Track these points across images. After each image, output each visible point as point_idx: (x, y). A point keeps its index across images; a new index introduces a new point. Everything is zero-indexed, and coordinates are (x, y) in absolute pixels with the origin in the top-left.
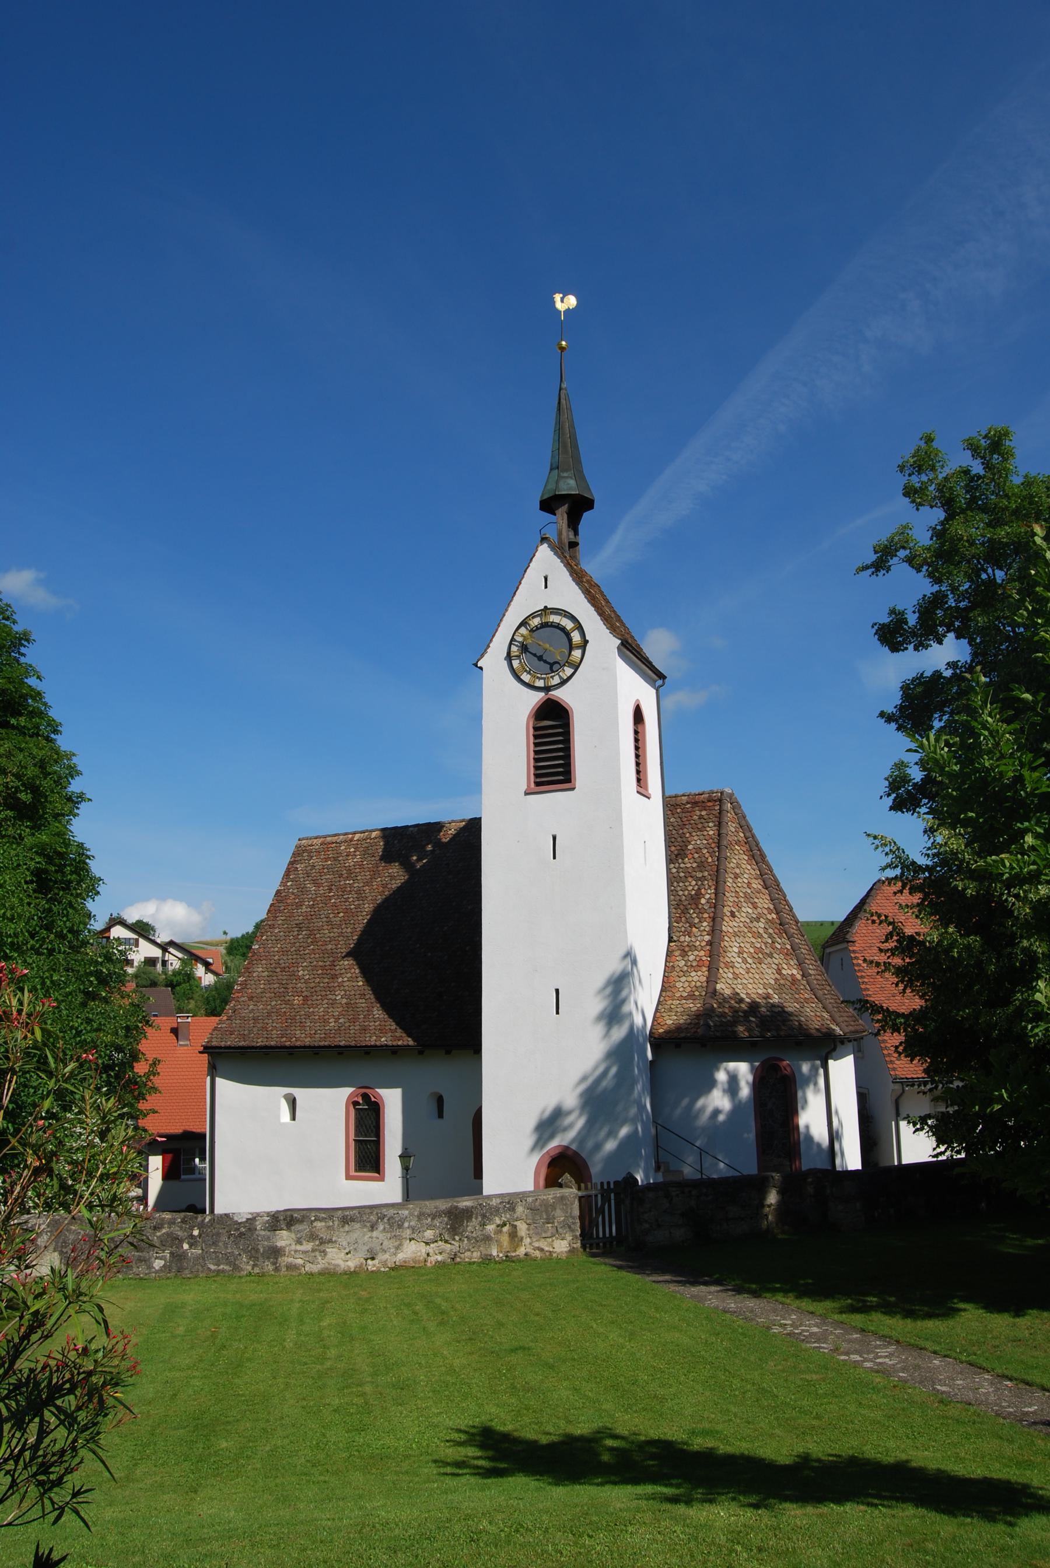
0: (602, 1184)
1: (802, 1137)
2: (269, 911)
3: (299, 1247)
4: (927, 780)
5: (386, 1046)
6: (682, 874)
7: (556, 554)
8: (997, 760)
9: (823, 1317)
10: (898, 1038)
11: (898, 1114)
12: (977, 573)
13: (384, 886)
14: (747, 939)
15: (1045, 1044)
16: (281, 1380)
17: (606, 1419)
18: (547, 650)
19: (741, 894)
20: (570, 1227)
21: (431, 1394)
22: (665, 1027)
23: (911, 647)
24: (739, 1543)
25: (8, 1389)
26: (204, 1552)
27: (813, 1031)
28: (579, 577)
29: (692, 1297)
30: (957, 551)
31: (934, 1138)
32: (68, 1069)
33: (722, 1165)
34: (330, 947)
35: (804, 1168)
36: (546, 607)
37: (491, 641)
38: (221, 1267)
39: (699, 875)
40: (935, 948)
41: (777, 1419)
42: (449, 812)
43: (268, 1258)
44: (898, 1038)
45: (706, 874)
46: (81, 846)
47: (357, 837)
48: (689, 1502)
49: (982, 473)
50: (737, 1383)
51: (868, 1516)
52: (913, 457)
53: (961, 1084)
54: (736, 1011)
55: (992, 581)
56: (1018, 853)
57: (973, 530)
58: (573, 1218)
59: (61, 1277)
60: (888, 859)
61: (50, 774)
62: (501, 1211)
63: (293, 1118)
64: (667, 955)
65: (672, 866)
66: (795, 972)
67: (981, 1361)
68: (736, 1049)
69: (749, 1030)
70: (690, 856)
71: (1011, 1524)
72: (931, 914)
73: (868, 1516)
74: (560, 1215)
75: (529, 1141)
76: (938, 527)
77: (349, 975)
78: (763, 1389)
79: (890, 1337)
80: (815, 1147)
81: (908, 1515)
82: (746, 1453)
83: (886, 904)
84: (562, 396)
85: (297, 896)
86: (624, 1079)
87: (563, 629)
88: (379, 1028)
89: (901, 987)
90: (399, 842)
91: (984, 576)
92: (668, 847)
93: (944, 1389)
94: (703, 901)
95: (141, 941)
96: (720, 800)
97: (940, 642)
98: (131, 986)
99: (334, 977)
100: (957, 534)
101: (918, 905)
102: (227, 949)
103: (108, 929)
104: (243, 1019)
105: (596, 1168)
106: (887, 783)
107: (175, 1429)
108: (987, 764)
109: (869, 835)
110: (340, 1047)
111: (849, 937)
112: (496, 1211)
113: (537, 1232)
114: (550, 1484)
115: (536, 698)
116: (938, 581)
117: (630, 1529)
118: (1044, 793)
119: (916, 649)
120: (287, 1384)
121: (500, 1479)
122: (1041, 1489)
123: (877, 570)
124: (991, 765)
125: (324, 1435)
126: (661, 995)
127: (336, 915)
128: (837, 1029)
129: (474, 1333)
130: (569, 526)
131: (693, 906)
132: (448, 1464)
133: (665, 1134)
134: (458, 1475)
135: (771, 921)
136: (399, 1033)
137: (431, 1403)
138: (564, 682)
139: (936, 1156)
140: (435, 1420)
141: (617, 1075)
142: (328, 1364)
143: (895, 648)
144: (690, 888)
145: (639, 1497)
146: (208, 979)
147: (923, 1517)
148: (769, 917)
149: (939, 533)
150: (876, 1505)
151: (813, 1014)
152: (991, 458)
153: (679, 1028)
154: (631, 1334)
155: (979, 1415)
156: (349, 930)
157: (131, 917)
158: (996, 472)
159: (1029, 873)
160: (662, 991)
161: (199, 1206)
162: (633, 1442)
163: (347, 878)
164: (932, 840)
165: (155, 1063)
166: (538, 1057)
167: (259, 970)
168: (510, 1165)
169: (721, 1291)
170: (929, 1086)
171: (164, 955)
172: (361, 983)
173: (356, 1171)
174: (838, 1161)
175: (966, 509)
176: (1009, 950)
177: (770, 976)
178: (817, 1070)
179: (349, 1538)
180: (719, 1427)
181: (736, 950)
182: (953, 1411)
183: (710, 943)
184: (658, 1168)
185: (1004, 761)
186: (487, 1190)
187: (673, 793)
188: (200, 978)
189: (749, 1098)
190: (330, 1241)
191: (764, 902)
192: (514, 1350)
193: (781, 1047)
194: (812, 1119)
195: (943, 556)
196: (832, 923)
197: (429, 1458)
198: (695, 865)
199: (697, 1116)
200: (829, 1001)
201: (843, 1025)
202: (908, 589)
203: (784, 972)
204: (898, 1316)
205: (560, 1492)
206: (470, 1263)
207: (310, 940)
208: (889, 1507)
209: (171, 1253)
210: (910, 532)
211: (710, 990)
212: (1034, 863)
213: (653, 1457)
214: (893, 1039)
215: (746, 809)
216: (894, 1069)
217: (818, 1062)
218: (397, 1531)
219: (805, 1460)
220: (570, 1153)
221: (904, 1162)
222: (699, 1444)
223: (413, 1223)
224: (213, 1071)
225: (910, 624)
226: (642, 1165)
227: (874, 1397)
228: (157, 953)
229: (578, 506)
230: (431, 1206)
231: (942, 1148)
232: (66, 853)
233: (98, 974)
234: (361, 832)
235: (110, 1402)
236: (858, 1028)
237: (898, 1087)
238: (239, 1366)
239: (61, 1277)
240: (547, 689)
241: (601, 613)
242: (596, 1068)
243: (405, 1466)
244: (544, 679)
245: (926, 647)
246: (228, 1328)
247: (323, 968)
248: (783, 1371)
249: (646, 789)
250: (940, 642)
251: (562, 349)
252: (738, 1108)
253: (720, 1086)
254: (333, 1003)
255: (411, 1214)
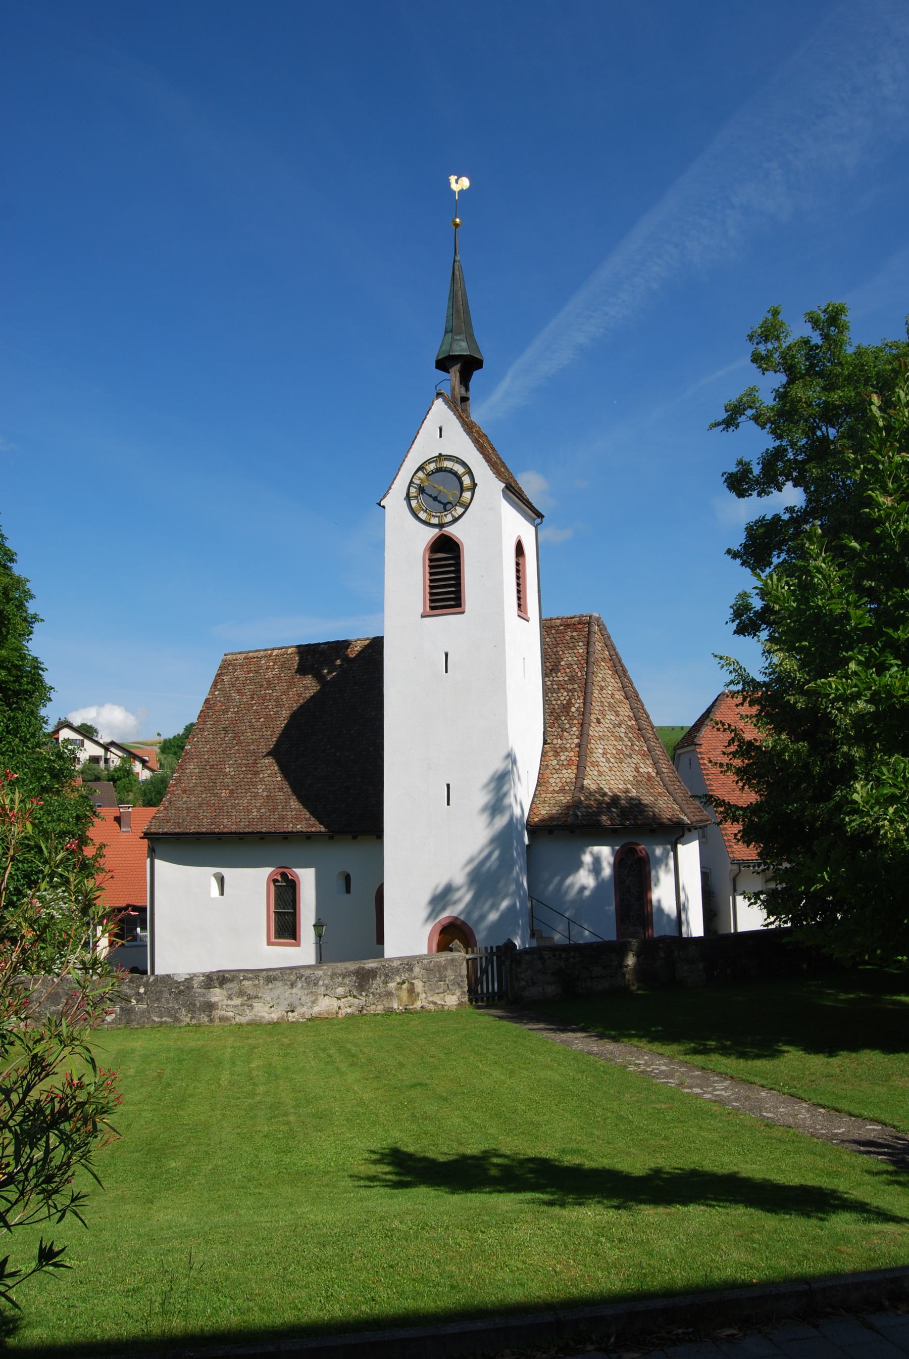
0: (486, 948)
1: (654, 910)
2: (199, 716)
3: (230, 1002)
4: (766, 609)
5: (302, 832)
6: (555, 687)
7: (449, 407)
8: (828, 599)
9: (671, 1058)
10: (737, 828)
11: (735, 890)
12: (813, 430)
13: (299, 695)
14: (610, 742)
15: (859, 833)
16: (218, 1112)
17: (491, 1141)
18: (441, 492)
19: (606, 704)
20: (459, 984)
21: (345, 1122)
22: (540, 816)
23: (755, 493)
24: (603, 1236)
25: (24, 1116)
26: (168, 1247)
27: (665, 821)
28: (469, 427)
29: (562, 1041)
30: (796, 411)
31: (765, 911)
32: (59, 857)
33: (587, 933)
34: (252, 747)
35: (655, 936)
36: (440, 454)
37: (393, 483)
38: (164, 1019)
39: (570, 687)
40: (769, 752)
41: (632, 1140)
42: (354, 631)
43: (204, 1011)
44: (737, 828)
45: (576, 686)
46: (35, 659)
47: (275, 652)
48: (563, 1205)
49: (820, 343)
50: (599, 1111)
51: (707, 1215)
52: (761, 327)
53: (789, 866)
54: (601, 804)
55: (825, 438)
56: (842, 677)
57: (810, 393)
58: (462, 977)
59: (57, 1026)
60: (732, 676)
61: (12, 600)
62: (401, 971)
63: (222, 894)
64: (542, 755)
65: (547, 679)
66: (650, 770)
67: (800, 1093)
68: (599, 835)
69: (611, 819)
70: (563, 671)
71: (822, 1219)
72: (767, 724)
73: (707, 1215)
74: (450, 975)
75: (424, 912)
76: (781, 390)
77: (269, 772)
78: (621, 1116)
79: (726, 1074)
80: (665, 918)
81: (740, 1213)
82: (607, 1167)
83: (729, 714)
84: (456, 268)
85: (223, 704)
86: (505, 863)
87: (455, 474)
88: (296, 817)
89: (741, 784)
90: (312, 657)
91: (819, 433)
92: (544, 663)
93: (769, 1115)
94: (573, 709)
95: (86, 742)
96: (589, 623)
97: (780, 490)
98: (79, 781)
99: (256, 773)
100: (797, 396)
101: (756, 716)
102: (160, 748)
103: (57, 731)
104: (177, 809)
105: (480, 935)
106: (731, 611)
107: (131, 1152)
108: (820, 603)
109: (716, 656)
110: (261, 833)
111: (697, 741)
112: (397, 971)
113: (431, 988)
114: (446, 1193)
115: (431, 534)
116: (780, 437)
117: (515, 1226)
118: (865, 628)
119: (759, 495)
120: (224, 1115)
121: (405, 1190)
122: (846, 1193)
123: (728, 426)
124: (823, 604)
125: (256, 1156)
126: (536, 789)
127: (258, 720)
128: (685, 818)
129: (379, 1072)
130: (461, 383)
131: (565, 714)
132: (362, 1178)
133: (539, 907)
134: (370, 1187)
135: (631, 727)
136: (313, 821)
137: (345, 1129)
138: (455, 520)
139: (767, 925)
140: (349, 1143)
141: (499, 858)
142: (258, 1098)
143: (741, 494)
144: (562, 698)
145: (521, 1202)
146: (145, 775)
147: (751, 1214)
148: (629, 723)
149: (782, 396)
150: (713, 1206)
151: (665, 806)
152: (829, 330)
153: (552, 818)
154: (511, 1072)
155: (797, 1136)
156: (269, 733)
157: (77, 723)
158: (832, 343)
159: (851, 694)
160: (537, 786)
161: (141, 968)
162: (514, 1160)
163: (267, 688)
164: (769, 661)
165: (102, 846)
166: (432, 840)
167: (191, 767)
168: (407, 932)
169: (586, 1037)
170: (762, 867)
171: (106, 754)
172: (279, 779)
173: (276, 938)
174: (684, 929)
175: (805, 374)
176: (831, 754)
177: (629, 774)
178: (668, 853)
179: (286, 1236)
180: (585, 1147)
181: (601, 751)
182: (776, 1133)
183: (579, 745)
184: (533, 935)
185: (834, 601)
186: (387, 955)
187: (548, 617)
188: (138, 774)
189: (611, 876)
190: (256, 997)
191: (625, 711)
192: (414, 1086)
193: (637, 832)
194: (663, 894)
195: (785, 415)
196: (682, 728)
197: (346, 1174)
198: (566, 678)
199: (566, 892)
200: (679, 795)
201: (691, 815)
202: (753, 443)
203: (641, 770)
204: (733, 1057)
205: (457, 1199)
206: (375, 1015)
207: (235, 742)
208: (724, 1207)
209: (121, 1008)
210: (757, 394)
211: (579, 785)
212: (856, 686)
213: (531, 1171)
214: (733, 828)
215: (610, 630)
216: (732, 852)
217: (669, 847)
218: (325, 1230)
219: (657, 1172)
220: (458, 922)
221: (739, 930)
222: (569, 1160)
223: (326, 982)
224: (152, 853)
225: (754, 474)
226: (520, 933)
227: (712, 1122)
228: (100, 752)
229: (469, 365)
230: (341, 967)
231: (772, 919)
232: (23, 665)
233: (51, 770)
234: (279, 649)
235: (100, 1126)
236: (703, 818)
237: (735, 867)
238: (182, 1100)
239: (57, 1026)
240: (441, 526)
241: (488, 460)
242: (481, 851)
243: (325, 1180)
244: (438, 517)
245: (768, 494)
246: (172, 1070)
247: (246, 765)
248: (637, 1101)
249: (526, 613)
250: (780, 490)
251: (456, 225)
252: (601, 886)
253: (586, 867)
254: (255, 796)
255: (325, 974)
